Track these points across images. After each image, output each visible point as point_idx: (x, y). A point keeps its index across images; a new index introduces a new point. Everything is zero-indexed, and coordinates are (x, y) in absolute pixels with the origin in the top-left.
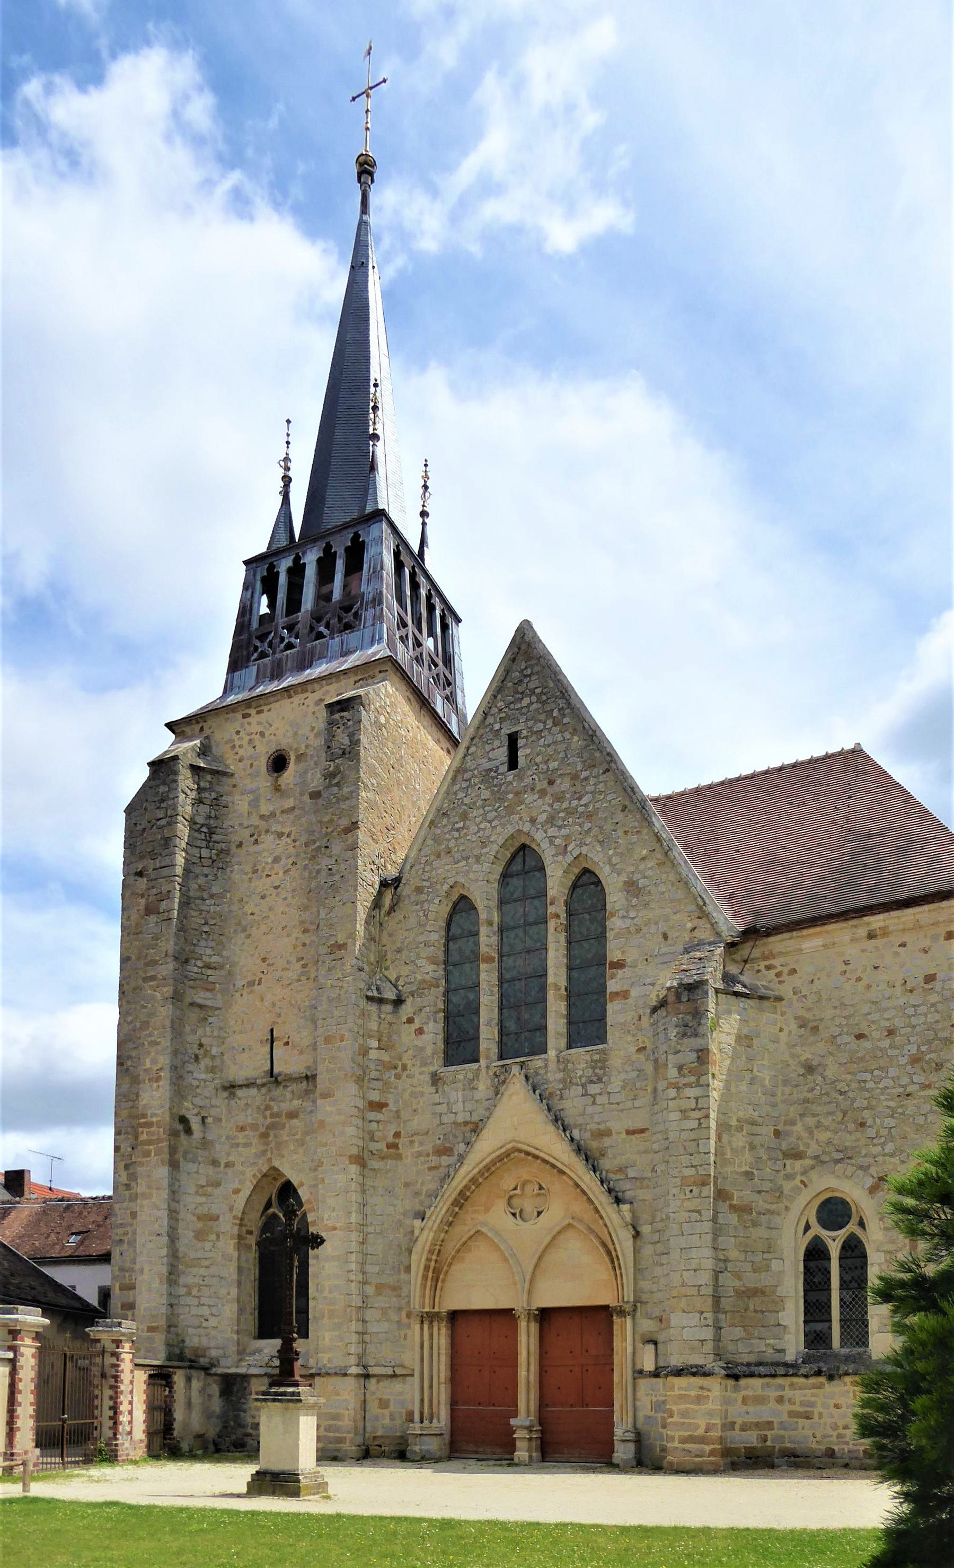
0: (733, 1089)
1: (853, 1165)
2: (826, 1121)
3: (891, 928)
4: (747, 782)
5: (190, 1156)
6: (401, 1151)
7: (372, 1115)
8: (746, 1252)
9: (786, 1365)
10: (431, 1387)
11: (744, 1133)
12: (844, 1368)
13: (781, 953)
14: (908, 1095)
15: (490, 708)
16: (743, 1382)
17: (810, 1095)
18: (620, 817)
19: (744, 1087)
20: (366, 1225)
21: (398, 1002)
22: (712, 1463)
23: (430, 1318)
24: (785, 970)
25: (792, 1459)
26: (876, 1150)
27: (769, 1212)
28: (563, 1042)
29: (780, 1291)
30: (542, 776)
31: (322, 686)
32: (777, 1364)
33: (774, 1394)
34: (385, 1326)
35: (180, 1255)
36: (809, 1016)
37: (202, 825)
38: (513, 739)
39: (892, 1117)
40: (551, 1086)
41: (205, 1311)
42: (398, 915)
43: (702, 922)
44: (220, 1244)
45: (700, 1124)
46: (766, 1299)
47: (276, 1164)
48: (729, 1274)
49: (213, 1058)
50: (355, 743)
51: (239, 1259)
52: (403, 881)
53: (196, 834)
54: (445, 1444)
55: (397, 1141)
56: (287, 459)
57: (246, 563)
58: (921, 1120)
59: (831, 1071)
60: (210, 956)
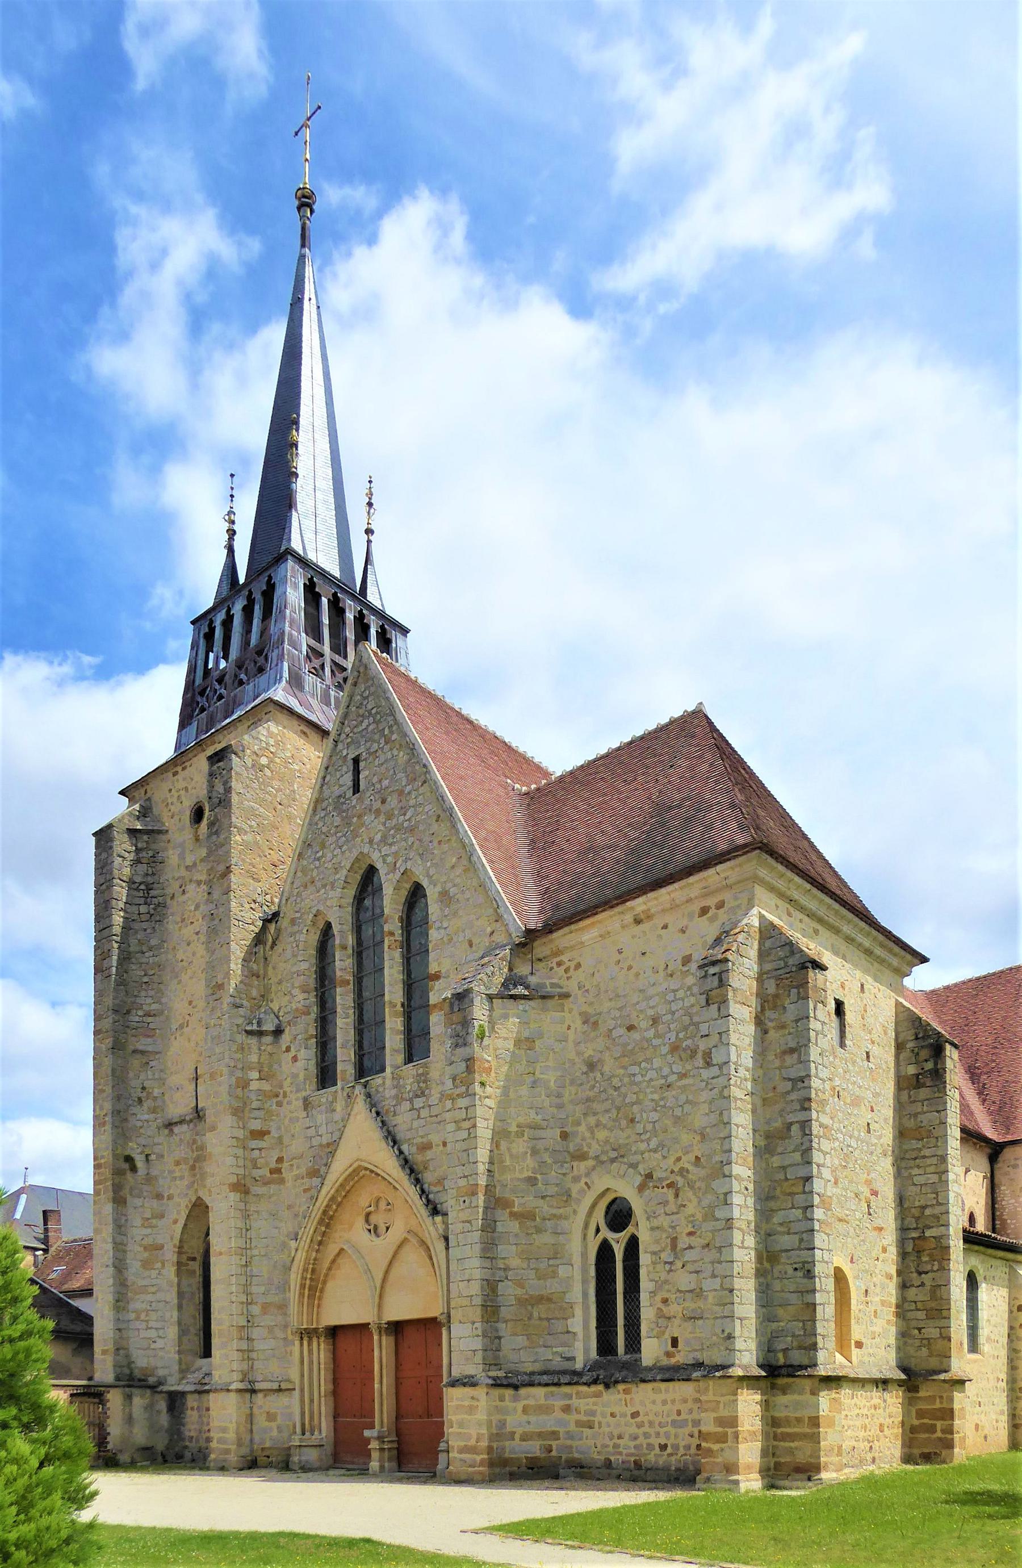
0: (512, 1095)
1: (625, 1164)
3: (653, 911)
4: (601, 762)
6: (284, 1175)
7: (254, 1144)
8: (529, 1259)
9: (574, 1373)
10: (312, 1401)
11: (526, 1138)
12: (618, 1376)
13: (572, 948)
14: (668, 1086)
15: (339, 735)
16: (523, 1391)
17: (591, 1094)
18: (435, 827)
19: (524, 1091)
20: (250, 1248)
21: (278, 1032)
22: (480, 1473)
23: (307, 1334)
24: (572, 965)
25: (578, 1470)
26: (643, 1146)
28: (400, 1058)
29: (568, 1298)
30: (377, 796)
31: (225, 736)
32: (564, 1372)
33: (559, 1403)
34: (272, 1343)
36: (590, 1010)
37: (140, 884)
38: (356, 761)
40: (387, 1103)
41: (152, 1334)
42: (279, 948)
43: (499, 924)
45: (469, 1134)
46: (552, 1306)
47: (201, 1194)
48: (510, 1283)
49: (155, 1098)
50: (228, 790)
51: (179, 1285)
52: (281, 915)
53: (136, 893)
54: (326, 1455)
56: (231, 512)
57: (193, 623)
58: (678, 1112)
59: (609, 1066)
60: (150, 1004)
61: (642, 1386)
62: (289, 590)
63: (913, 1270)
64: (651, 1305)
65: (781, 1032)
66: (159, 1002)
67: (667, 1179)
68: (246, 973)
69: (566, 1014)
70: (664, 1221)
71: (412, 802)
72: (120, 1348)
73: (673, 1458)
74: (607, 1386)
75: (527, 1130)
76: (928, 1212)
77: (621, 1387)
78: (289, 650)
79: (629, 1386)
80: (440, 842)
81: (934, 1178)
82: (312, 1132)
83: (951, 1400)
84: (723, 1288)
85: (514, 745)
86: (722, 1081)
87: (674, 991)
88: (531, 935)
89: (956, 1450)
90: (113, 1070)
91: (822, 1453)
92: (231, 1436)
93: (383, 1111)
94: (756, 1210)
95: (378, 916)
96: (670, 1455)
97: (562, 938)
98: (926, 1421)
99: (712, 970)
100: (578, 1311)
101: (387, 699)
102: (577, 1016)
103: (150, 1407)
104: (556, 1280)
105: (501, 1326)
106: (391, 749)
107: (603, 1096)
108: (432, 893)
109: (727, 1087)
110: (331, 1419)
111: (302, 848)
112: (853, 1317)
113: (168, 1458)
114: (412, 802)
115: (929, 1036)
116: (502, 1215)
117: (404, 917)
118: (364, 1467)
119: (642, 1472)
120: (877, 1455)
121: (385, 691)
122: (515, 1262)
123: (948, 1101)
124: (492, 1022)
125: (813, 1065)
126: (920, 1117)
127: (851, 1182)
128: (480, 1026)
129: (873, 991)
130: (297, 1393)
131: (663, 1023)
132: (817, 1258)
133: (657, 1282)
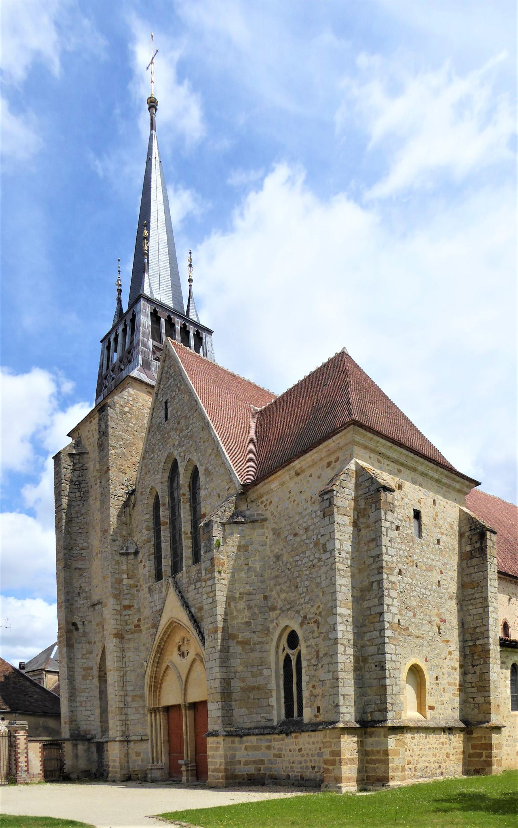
0: (236, 577)
2: (284, 587)
5: (78, 641)
6: (142, 628)
7: (126, 612)
9: (273, 728)
10: (157, 745)
12: (292, 729)
13: (267, 493)
16: (245, 738)
19: (243, 575)
20: (125, 667)
21: (136, 553)
22: (221, 783)
23: (154, 711)
24: (268, 502)
25: (275, 780)
26: (302, 601)
27: (261, 643)
28: (190, 562)
33: (264, 744)
34: (137, 716)
35: (76, 687)
37: (76, 481)
38: (166, 403)
39: (307, 580)
41: (89, 713)
42: (136, 509)
43: (231, 483)
44: (93, 681)
45: (213, 600)
46: (261, 691)
48: (237, 680)
50: (107, 426)
51: (100, 687)
53: (74, 487)
55: (139, 623)
59: (286, 557)
60: (82, 544)
61: (303, 734)
62: (142, 316)
63: (470, 664)
64: (307, 689)
65: (368, 530)
66: (87, 542)
67: (313, 618)
68: (119, 523)
69: (265, 530)
70: (312, 642)
71: (191, 422)
72: (72, 721)
73: (318, 774)
74: (287, 735)
75: (245, 596)
76: (477, 630)
77: (293, 735)
78: (142, 350)
79: (297, 734)
80: (204, 441)
81: (481, 611)
82: (152, 604)
83: (491, 738)
84: (333, 678)
85: (261, 387)
86: (331, 560)
87: (315, 512)
88: (246, 487)
89: (494, 767)
90: (65, 578)
91: (390, 771)
92: (117, 764)
93: (182, 591)
94: (354, 633)
95: (179, 487)
96: (317, 772)
97: (261, 488)
98: (477, 751)
99: (326, 497)
100: (274, 694)
101: (178, 367)
102: (271, 531)
103: (88, 750)
104: (262, 677)
105: (233, 703)
106: (181, 394)
107: (283, 574)
108: (201, 470)
109: (334, 563)
110: (167, 755)
111: (144, 454)
112: (427, 693)
113: (97, 776)
114: (191, 422)
115: (478, 528)
116: (232, 643)
117: (191, 485)
118: (179, 780)
119: (304, 782)
120: (444, 771)
121: (177, 362)
122: (240, 668)
123: (489, 565)
124: (224, 538)
125: (384, 548)
126: (473, 575)
127: (426, 615)
128: (218, 540)
129: (442, 503)
130: (150, 741)
131: (311, 530)
132: (387, 659)
133: (309, 676)
